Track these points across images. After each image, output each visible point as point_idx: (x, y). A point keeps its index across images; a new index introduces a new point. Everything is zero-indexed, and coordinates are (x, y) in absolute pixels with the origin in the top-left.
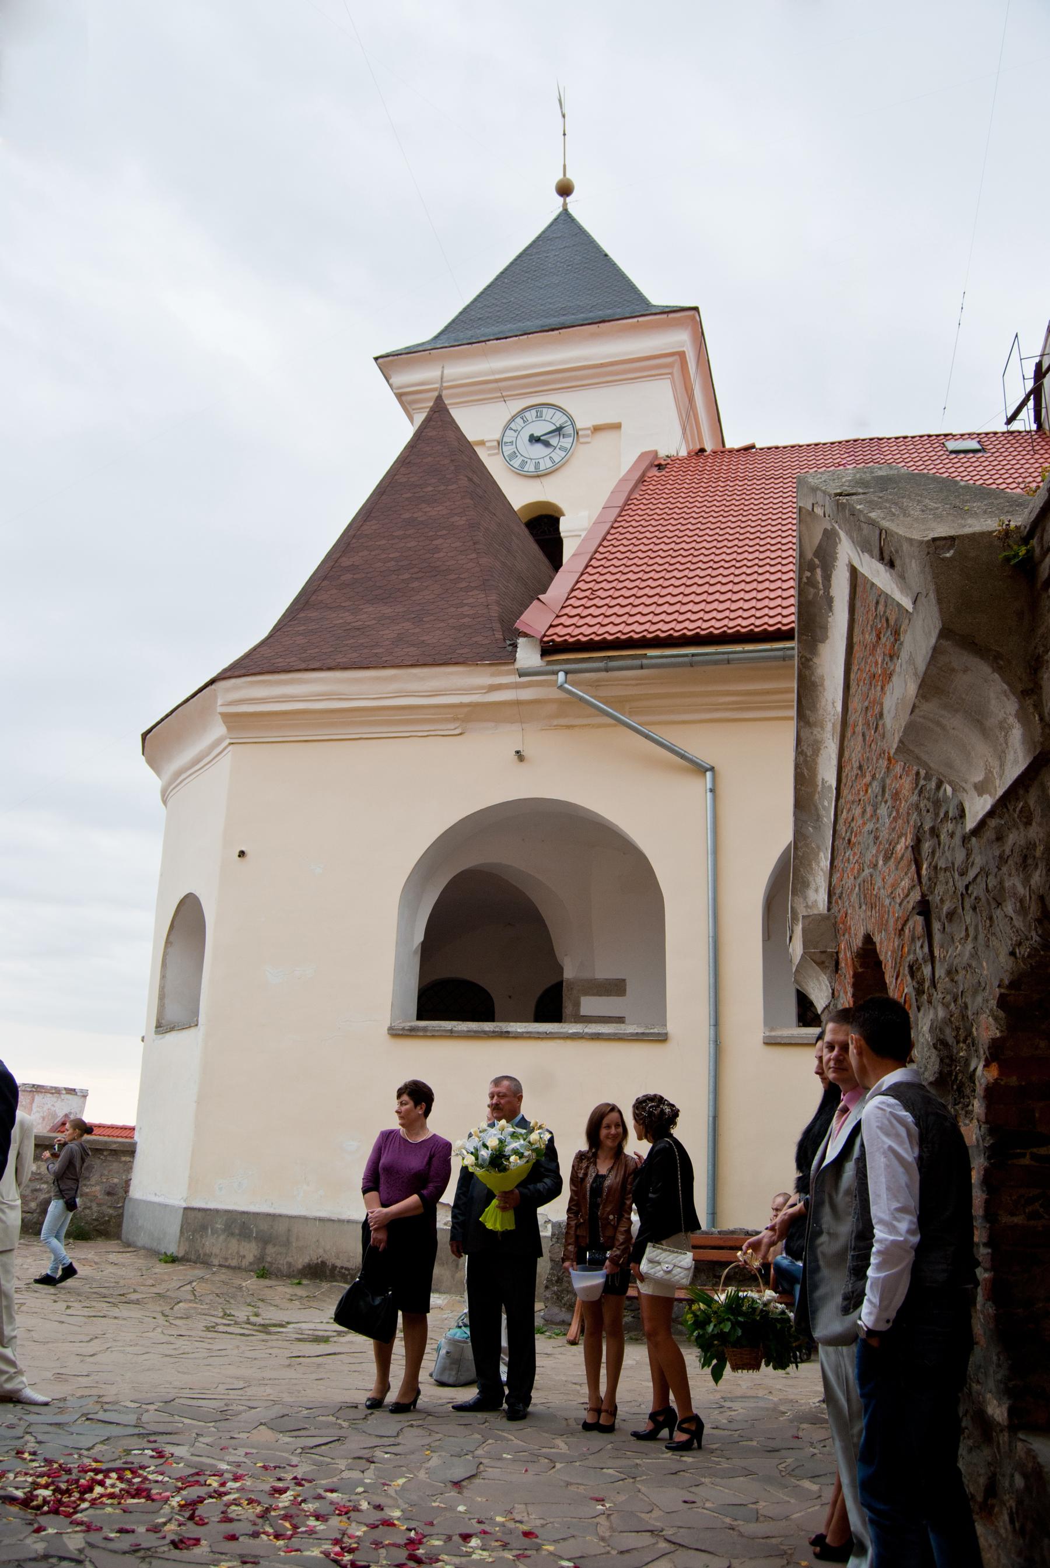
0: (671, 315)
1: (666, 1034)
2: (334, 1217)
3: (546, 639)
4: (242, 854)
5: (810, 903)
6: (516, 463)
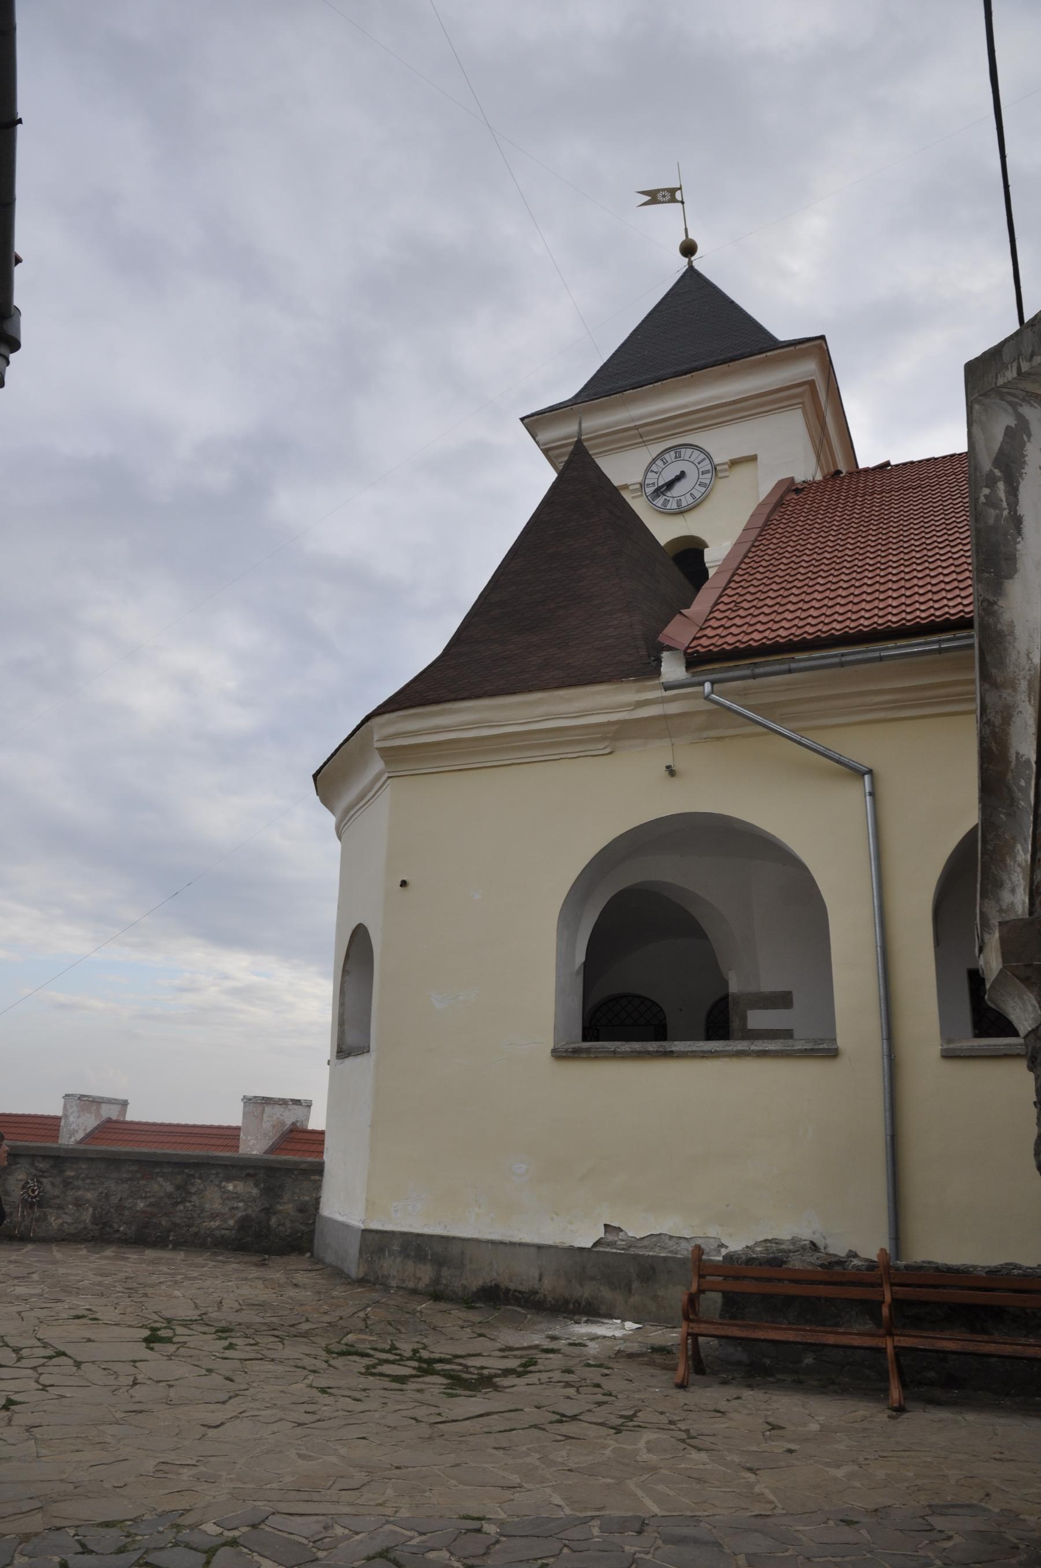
0: (798, 347)
1: (837, 1049)
2: (506, 1239)
3: (689, 651)
4: (404, 884)
5: (1004, 907)
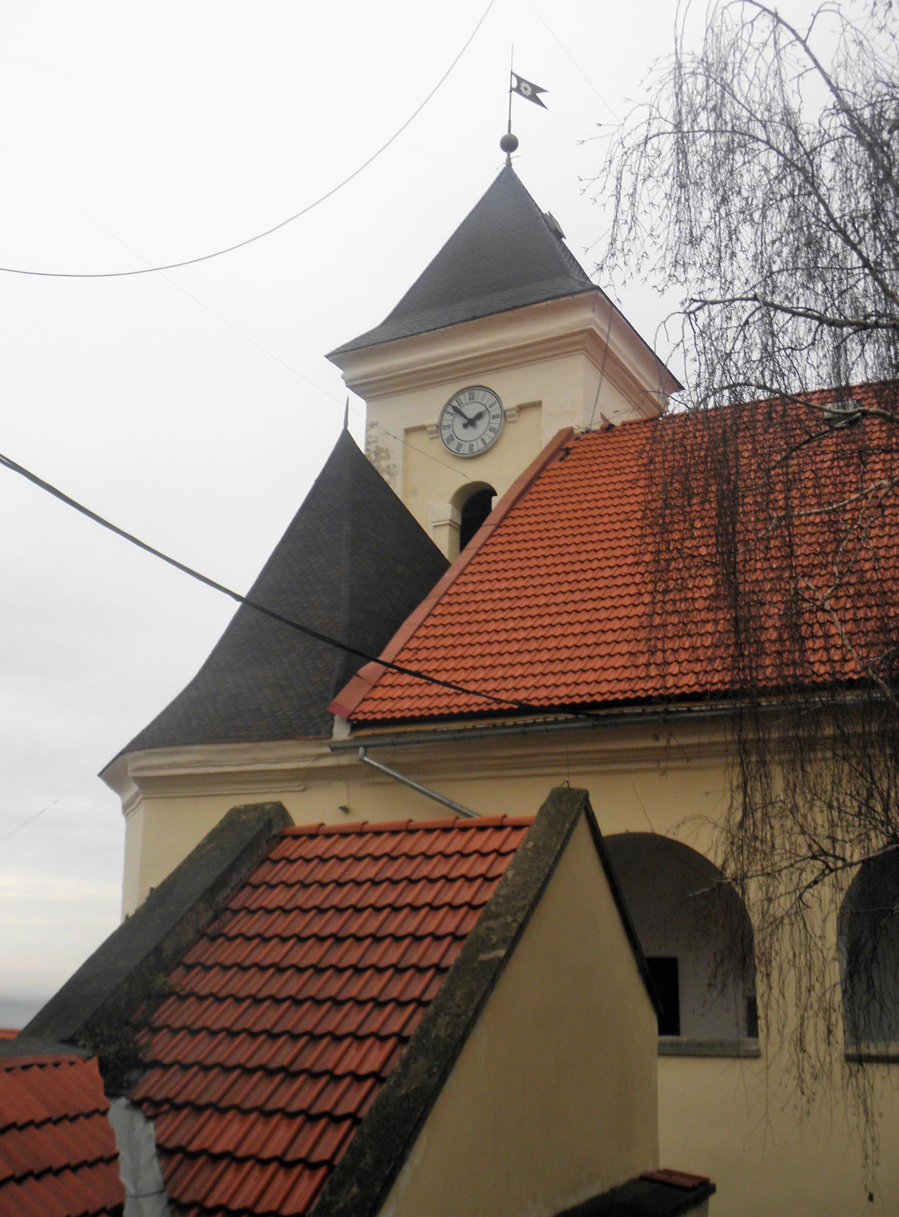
0: (577, 296)
3: (352, 718)
6: (453, 446)
